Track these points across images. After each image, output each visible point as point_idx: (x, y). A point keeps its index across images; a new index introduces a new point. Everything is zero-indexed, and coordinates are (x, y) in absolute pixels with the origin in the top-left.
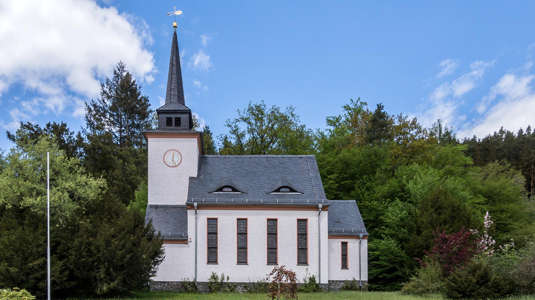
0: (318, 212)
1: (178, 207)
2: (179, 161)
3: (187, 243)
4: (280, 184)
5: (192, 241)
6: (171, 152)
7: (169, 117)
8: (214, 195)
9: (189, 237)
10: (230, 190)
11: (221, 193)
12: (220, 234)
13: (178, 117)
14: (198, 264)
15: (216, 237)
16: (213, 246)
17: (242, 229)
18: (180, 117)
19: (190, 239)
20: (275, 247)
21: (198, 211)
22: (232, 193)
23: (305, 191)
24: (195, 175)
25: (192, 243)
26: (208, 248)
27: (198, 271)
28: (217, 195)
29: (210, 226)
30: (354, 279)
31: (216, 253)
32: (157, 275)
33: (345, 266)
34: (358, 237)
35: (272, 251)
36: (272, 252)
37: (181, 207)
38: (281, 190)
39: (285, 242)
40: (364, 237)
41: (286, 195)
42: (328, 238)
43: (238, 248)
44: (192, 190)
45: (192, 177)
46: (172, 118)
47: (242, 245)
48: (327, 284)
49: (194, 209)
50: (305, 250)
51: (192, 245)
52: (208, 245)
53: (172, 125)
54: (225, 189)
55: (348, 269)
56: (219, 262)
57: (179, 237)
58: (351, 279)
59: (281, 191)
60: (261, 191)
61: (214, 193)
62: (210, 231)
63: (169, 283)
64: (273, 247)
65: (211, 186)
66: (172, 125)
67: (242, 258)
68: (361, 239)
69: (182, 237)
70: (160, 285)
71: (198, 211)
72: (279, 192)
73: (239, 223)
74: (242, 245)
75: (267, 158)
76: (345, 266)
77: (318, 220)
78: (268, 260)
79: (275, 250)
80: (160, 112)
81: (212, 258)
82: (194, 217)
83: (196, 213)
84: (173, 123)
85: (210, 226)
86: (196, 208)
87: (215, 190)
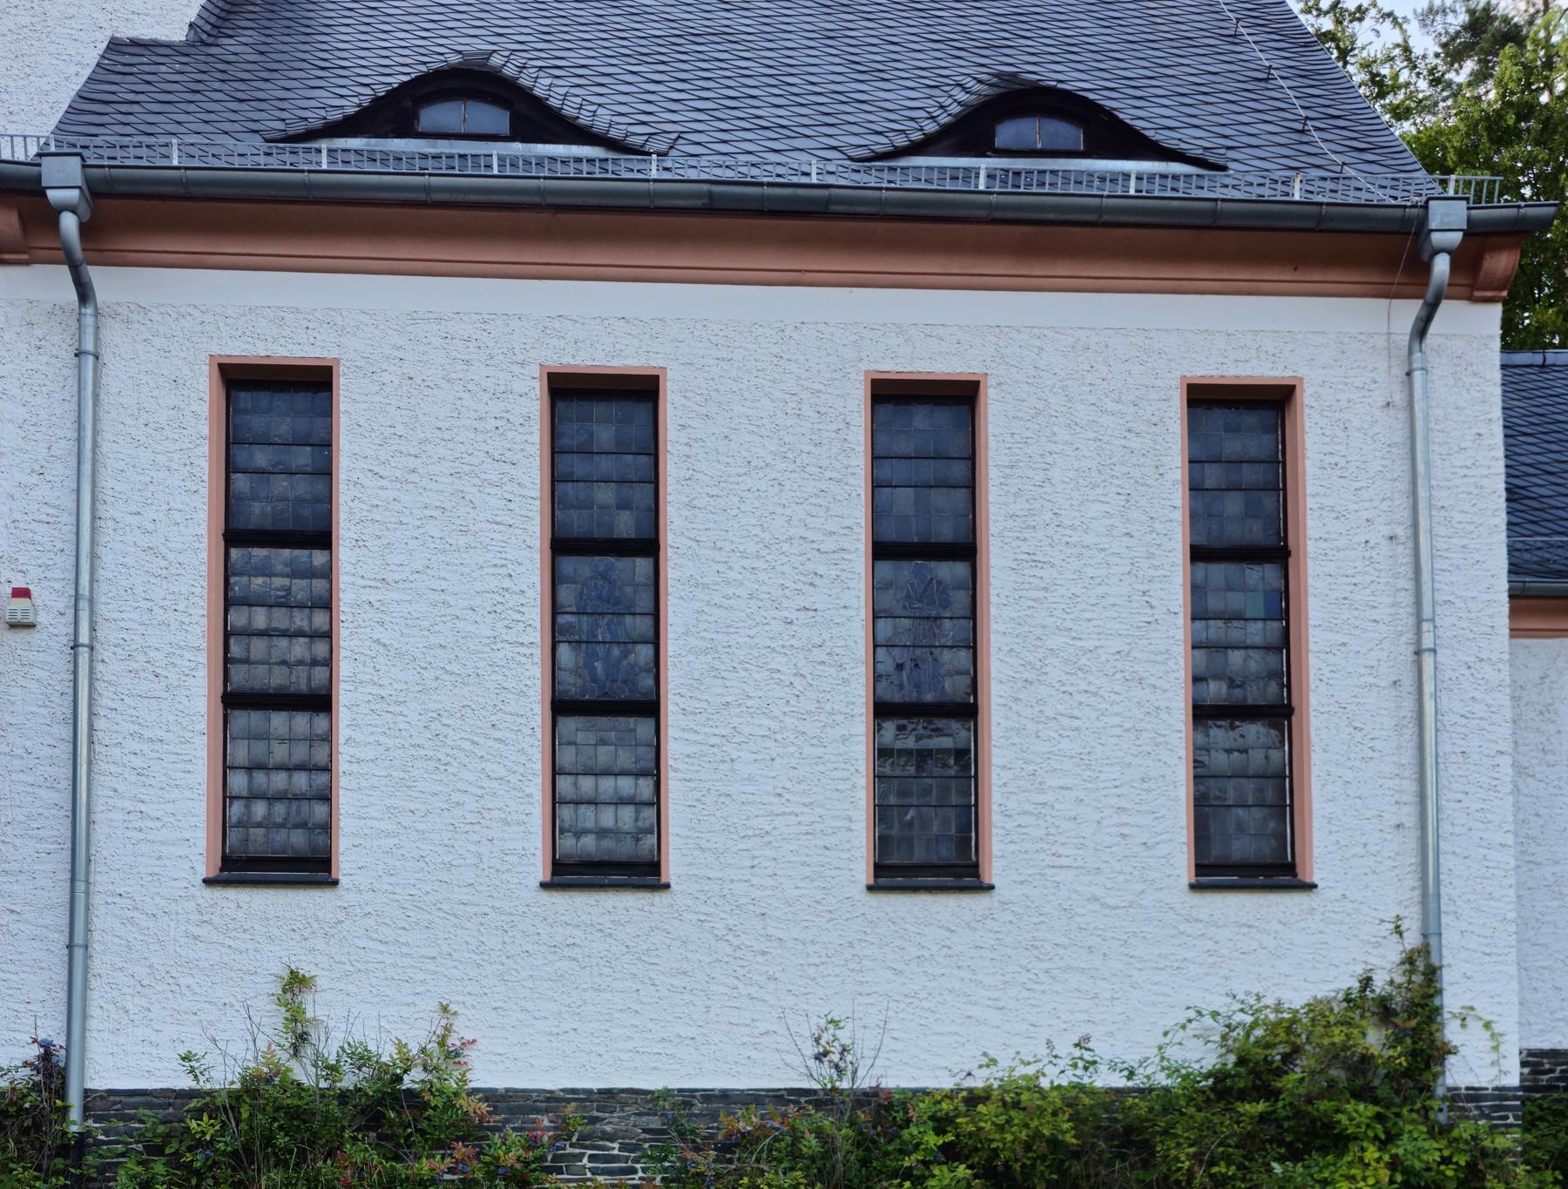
5: (42, 618)
22: (517, 148)
44: (105, 119)
62: (257, 513)
71: (98, 276)
72: (407, 129)
77: (1399, 398)
83: (84, 293)
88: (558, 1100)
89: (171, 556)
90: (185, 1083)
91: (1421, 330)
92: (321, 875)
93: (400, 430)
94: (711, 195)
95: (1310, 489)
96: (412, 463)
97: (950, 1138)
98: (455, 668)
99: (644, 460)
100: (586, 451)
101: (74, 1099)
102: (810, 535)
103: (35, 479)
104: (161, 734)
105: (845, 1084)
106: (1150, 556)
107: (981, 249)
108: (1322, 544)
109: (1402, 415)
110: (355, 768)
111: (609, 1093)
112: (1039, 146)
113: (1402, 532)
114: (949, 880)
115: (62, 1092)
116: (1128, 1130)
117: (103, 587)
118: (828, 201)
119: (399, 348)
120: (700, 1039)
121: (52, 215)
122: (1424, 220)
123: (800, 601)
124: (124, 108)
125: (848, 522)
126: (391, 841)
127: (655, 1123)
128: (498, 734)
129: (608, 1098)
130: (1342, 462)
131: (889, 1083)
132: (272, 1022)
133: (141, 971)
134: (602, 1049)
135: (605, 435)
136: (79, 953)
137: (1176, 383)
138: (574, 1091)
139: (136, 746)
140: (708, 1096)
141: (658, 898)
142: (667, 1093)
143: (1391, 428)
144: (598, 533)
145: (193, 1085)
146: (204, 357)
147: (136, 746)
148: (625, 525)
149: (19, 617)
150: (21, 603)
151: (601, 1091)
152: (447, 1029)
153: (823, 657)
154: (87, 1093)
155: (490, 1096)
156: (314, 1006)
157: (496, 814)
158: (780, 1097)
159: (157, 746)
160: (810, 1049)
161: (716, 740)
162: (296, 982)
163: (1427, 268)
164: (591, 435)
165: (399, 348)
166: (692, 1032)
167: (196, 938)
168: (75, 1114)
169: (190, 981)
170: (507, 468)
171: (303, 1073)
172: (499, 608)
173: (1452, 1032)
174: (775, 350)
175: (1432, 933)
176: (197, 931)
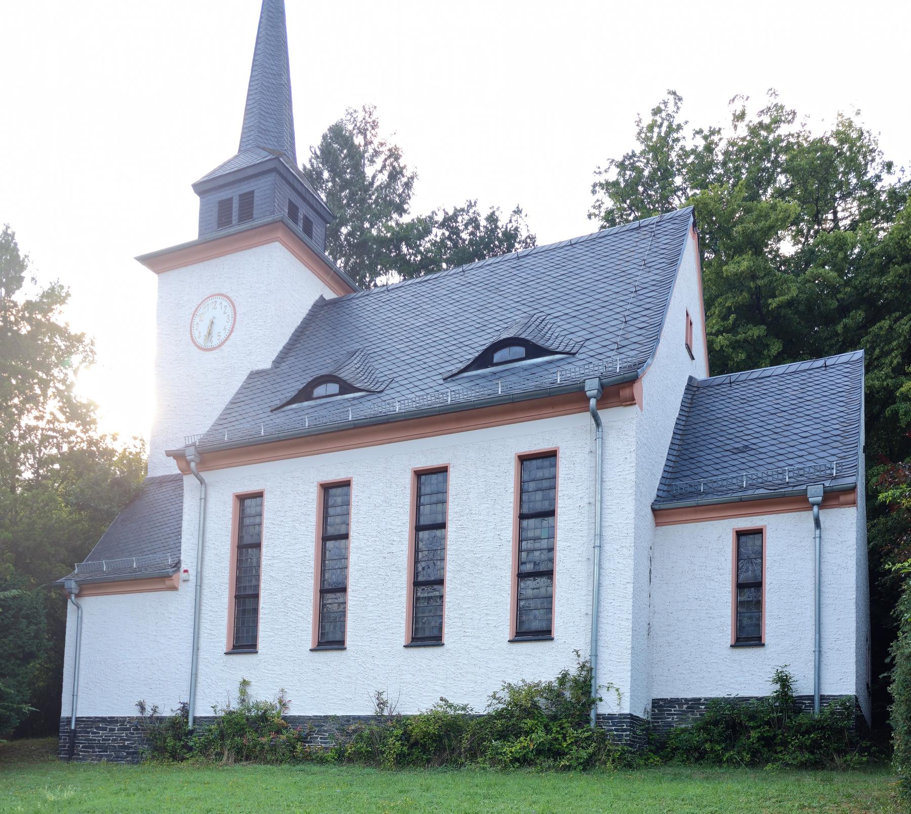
2: (229, 326)
3: (174, 588)
4: (483, 342)
8: (292, 412)
9: (184, 566)
10: (520, 351)
11: (306, 404)
14: (202, 654)
19: (186, 571)
21: (605, 415)
30: (382, 704)
32: (488, 698)
38: (498, 357)
49: (586, 409)
51: (186, 592)
54: (319, 391)
58: (368, 709)
59: (495, 361)
63: (124, 721)
68: (816, 509)
70: (105, 729)
71: (602, 414)
72: (309, 398)
73: (258, 509)
80: (282, 170)
86: (593, 402)
88: (312, 719)
90: (212, 714)
92: (340, 647)
96: (282, 519)
98: (291, 582)
102: (392, 527)
103: (190, 537)
106: (502, 521)
108: (563, 509)
111: (326, 717)
114: (433, 642)
115: (187, 717)
118: (388, 419)
122: (584, 387)
123: (388, 550)
125: (404, 522)
129: (326, 718)
130: (572, 477)
131: (403, 714)
132: (236, 694)
138: (316, 716)
141: (343, 653)
144: (336, 533)
147: (210, 614)
151: (324, 716)
153: (395, 569)
154: (195, 719)
157: (300, 628)
161: (362, 599)
164: (335, 501)
168: (190, 724)
173: (603, 693)
174: (385, 466)
175: (595, 655)
176: (223, 668)
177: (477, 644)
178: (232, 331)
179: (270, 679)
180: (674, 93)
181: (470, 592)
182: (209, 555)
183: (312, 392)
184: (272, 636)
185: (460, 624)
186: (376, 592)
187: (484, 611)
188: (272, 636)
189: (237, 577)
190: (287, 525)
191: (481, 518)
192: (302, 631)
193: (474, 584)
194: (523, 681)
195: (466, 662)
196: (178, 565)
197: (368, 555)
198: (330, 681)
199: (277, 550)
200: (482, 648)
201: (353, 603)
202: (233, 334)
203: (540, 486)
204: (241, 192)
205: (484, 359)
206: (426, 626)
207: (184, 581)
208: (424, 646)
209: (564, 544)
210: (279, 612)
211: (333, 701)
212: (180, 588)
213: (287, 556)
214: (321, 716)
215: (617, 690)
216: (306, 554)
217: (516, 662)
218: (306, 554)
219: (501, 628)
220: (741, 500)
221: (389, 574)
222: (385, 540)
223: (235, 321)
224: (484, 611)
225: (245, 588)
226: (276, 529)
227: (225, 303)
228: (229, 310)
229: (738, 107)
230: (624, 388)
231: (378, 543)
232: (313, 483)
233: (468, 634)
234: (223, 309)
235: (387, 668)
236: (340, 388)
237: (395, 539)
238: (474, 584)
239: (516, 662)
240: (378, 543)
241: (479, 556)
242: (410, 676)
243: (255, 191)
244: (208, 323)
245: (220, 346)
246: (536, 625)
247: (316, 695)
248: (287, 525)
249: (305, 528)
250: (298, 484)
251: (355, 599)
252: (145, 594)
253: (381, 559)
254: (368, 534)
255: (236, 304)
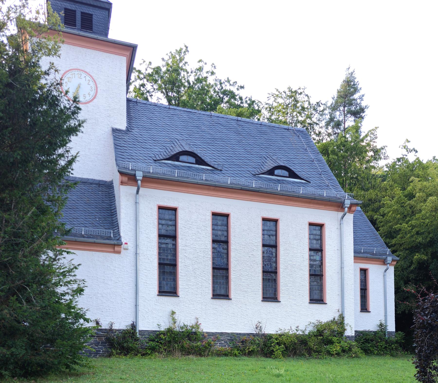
0: (341, 214)
1: (91, 184)
2: (92, 93)
3: (119, 252)
4: (178, 149)
5: (129, 248)
6: (77, 73)
7: (69, 8)
10: (193, 160)
12: (182, 239)
13: (87, 12)
14: (140, 294)
15: (173, 244)
16: (168, 262)
17: (220, 233)
18: (90, 13)
19: (126, 244)
20: (273, 270)
22: (197, 166)
23: (310, 179)
24: (122, 125)
25: (128, 251)
26: (160, 264)
27: (140, 308)
28: (170, 165)
29: (163, 222)
31: (227, 278)
33: (364, 308)
34: (384, 262)
35: (268, 277)
36: (269, 279)
37: (96, 184)
39: (290, 263)
40: (390, 264)
41: (285, 182)
42: (354, 262)
43: (214, 268)
44: (122, 151)
45: (117, 130)
46: (75, 11)
47: (219, 263)
48: (352, 336)
50: (319, 278)
52: (159, 259)
53: (75, 25)
55: (179, 296)
56: (180, 292)
57: (102, 238)
60: (242, 169)
61: (164, 161)
62: (163, 232)
64: (270, 270)
65: (156, 150)
66: (75, 25)
67: (220, 288)
68: (388, 265)
69: (109, 238)
71: (141, 190)
72: (178, 160)
74: (221, 263)
75: (237, 120)
76: (364, 308)
77: (339, 227)
78: (160, 287)
79: (273, 275)
81: (167, 284)
82: (132, 201)
83: (138, 192)
84: (77, 22)
85: (163, 222)
87: (168, 157)
88: (214, 334)
89: (151, 239)
90: (157, 329)
91: (342, 218)
93: (188, 220)
94: (241, 188)
95: (326, 241)
96: (190, 226)
97: (278, 341)
98: (197, 261)
99: (226, 227)
100: (217, 225)
101: (137, 331)
103: (127, 223)
104: (150, 269)
105: (260, 333)
107: (279, 199)
109: (339, 230)
110: (181, 277)
111: (222, 333)
112: (281, 175)
113: (339, 248)
115: (135, 330)
116: (128, 353)
117: (140, 243)
119: (188, 206)
120: (236, 325)
121: (136, 180)
122: (344, 202)
123: (251, 253)
124: (124, 148)
125: (259, 241)
126: (188, 290)
127: (229, 338)
128: (204, 273)
129: (222, 334)
133: (147, 310)
134: (221, 326)
135: (220, 223)
136: (138, 306)
137: (307, 222)
138: (216, 332)
139: (145, 271)
140: (237, 334)
141: (230, 301)
142: (232, 333)
143: (337, 232)
145: (158, 329)
146: (156, 204)
147: (145, 271)
148: (223, 239)
149: (126, 248)
150: (126, 245)
151: (221, 333)
152: (198, 322)
153: (255, 263)
154: (140, 331)
155: (207, 333)
156: (176, 316)
158: (249, 334)
159: (149, 271)
160: (255, 327)
161: (238, 275)
162: (173, 313)
163: (344, 209)
165: (188, 206)
166: (235, 323)
167: (156, 305)
168: (138, 334)
169: (155, 312)
170: (206, 228)
171: (177, 329)
172: (204, 251)
176: (156, 304)
177: (295, 303)
178: (95, 98)
179: (187, 312)
180: (187, 47)
181: (291, 279)
182: (142, 238)
183: (179, 158)
184: (187, 289)
185: (287, 293)
186: (246, 273)
187: (298, 289)
188: (187, 289)
189: (159, 253)
190: (193, 230)
191: (295, 246)
192: (206, 287)
193: (292, 276)
194: (200, 324)
195: (291, 311)
196: (120, 239)
197: (241, 254)
198: (223, 315)
199: (188, 242)
200: (298, 305)
201: (234, 277)
202: (95, 100)
203: (315, 237)
204: (82, 11)
205: (175, 157)
206: (268, 292)
207: (124, 249)
208: (269, 301)
209: (329, 264)
210: (191, 276)
211: (225, 325)
212: (121, 253)
213: (194, 247)
214: (219, 333)
215: (350, 326)
216: (206, 247)
217: (312, 312)
218: (206, 247)
219: (305, 297)
220: (367, 258)
221: (252, 265)
222: (249, 248)
223: (97, 92)
224: (298, 289)
225: (164, 259)
226: (187, 231)
227: (88, 78)
228: (92, 84)
229: (201, 64)
230: (353, 206)
231: (246, 249)
232: (208, 210)
233: (291, 298)
234: (87, 82)
235: (253, 310)
236: (196, 161)
237: (255, 248)
238: (292, 276)
239: (312, 312)
240: (246, 249)
241: (295, 263)
242: (265, 315)
243: (94, 16)
244: (76, 85)
245: (85, 103)
246: (316, 297)
247: (215, 322)
248: (193, 230)
249: (205, 234)
250: (199, 209)
251: (235, 275)
252: (94, 252)
253: (248, 257)
254: (240, 244)
255: (97, 82)
